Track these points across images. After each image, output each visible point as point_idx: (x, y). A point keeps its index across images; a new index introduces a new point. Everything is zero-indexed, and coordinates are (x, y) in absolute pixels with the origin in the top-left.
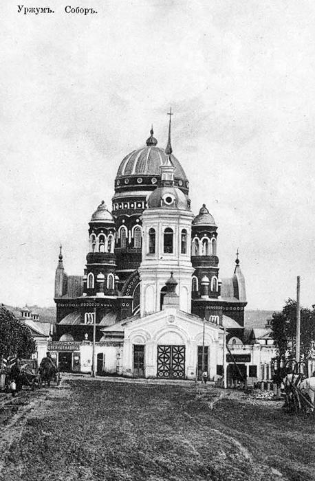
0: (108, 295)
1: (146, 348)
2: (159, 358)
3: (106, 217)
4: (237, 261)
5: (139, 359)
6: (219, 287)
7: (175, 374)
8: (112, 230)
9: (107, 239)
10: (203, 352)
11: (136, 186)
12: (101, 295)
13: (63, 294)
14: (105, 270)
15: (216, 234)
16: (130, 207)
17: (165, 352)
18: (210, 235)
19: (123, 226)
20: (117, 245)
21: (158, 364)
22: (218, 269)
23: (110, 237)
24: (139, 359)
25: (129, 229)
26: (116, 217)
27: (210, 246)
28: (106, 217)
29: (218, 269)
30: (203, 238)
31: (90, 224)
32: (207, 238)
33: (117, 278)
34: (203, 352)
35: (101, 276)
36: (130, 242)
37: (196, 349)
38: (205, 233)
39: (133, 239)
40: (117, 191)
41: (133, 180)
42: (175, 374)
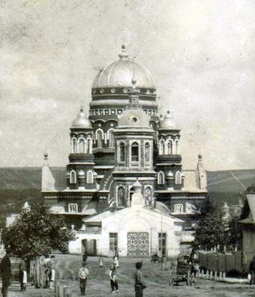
0: (89, 188)
1: (119, 235)
2: (129, 242)
3: (85, 123)
4: (200, 157)
5: (114, 246)
6: (182, 180)
7: (141, 254)
8: (91, 134)
9: (86, 141)
10: (163, 236)
11: (109, 95)
12: (82, 189)
13: (100, 190)
14: (85, 168)
15: (179, 136)
16: (115, 111)
17: (144, 238)
18: (173, 137)
19: (100, 129)
20: (94, 146)
21: (128, 246)
22: (181, 166)
23: (89, 140)
24: (114, 246)
25: (105, 132)
26: (94, 122)
27: (174, 147)
28: (85, 123)
29: (181, 166)
30: (80, 138)
31: (71, 129)
32: (83, 138)
33: (95, 174)
34: (163, 236)
35: (82, 173)
36: (106, 142)
37: (116, 232)
38: (169, 135)
39: (108, 141)
40: (94, 99)
41: (108, 90)
42: (141, 254)
